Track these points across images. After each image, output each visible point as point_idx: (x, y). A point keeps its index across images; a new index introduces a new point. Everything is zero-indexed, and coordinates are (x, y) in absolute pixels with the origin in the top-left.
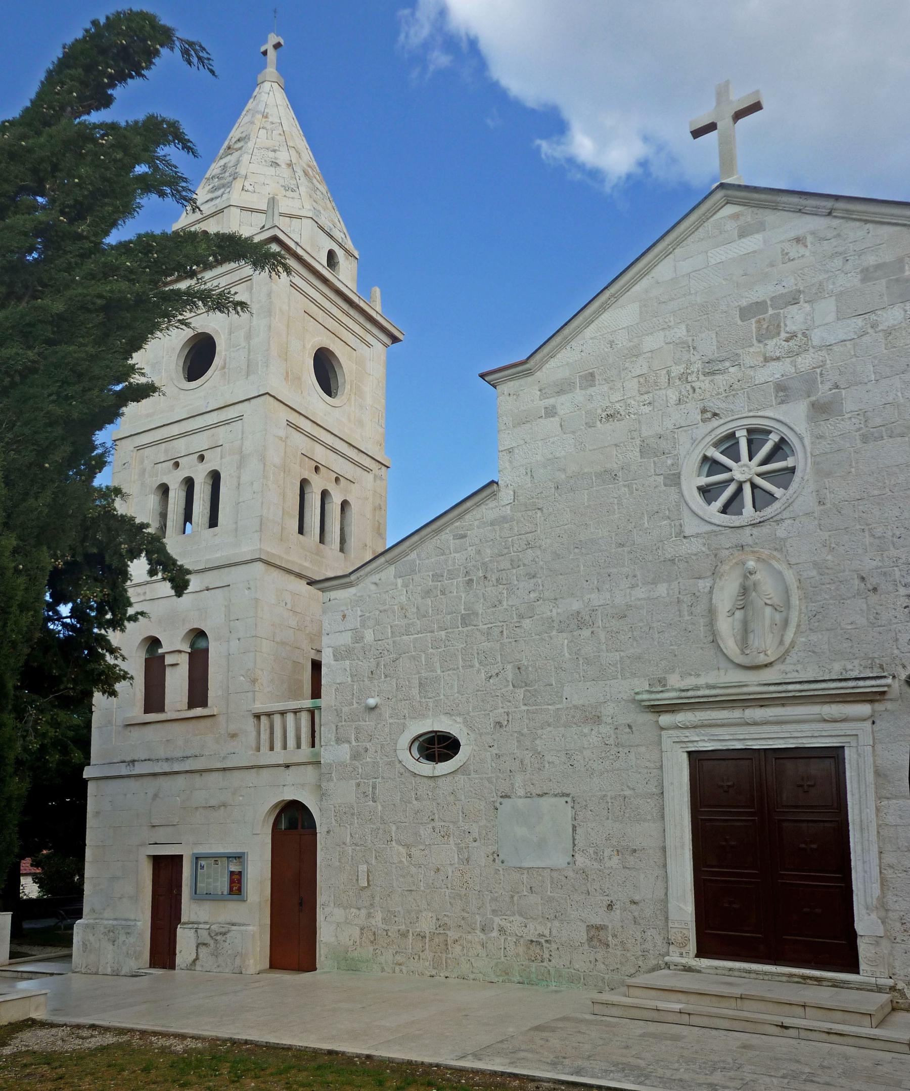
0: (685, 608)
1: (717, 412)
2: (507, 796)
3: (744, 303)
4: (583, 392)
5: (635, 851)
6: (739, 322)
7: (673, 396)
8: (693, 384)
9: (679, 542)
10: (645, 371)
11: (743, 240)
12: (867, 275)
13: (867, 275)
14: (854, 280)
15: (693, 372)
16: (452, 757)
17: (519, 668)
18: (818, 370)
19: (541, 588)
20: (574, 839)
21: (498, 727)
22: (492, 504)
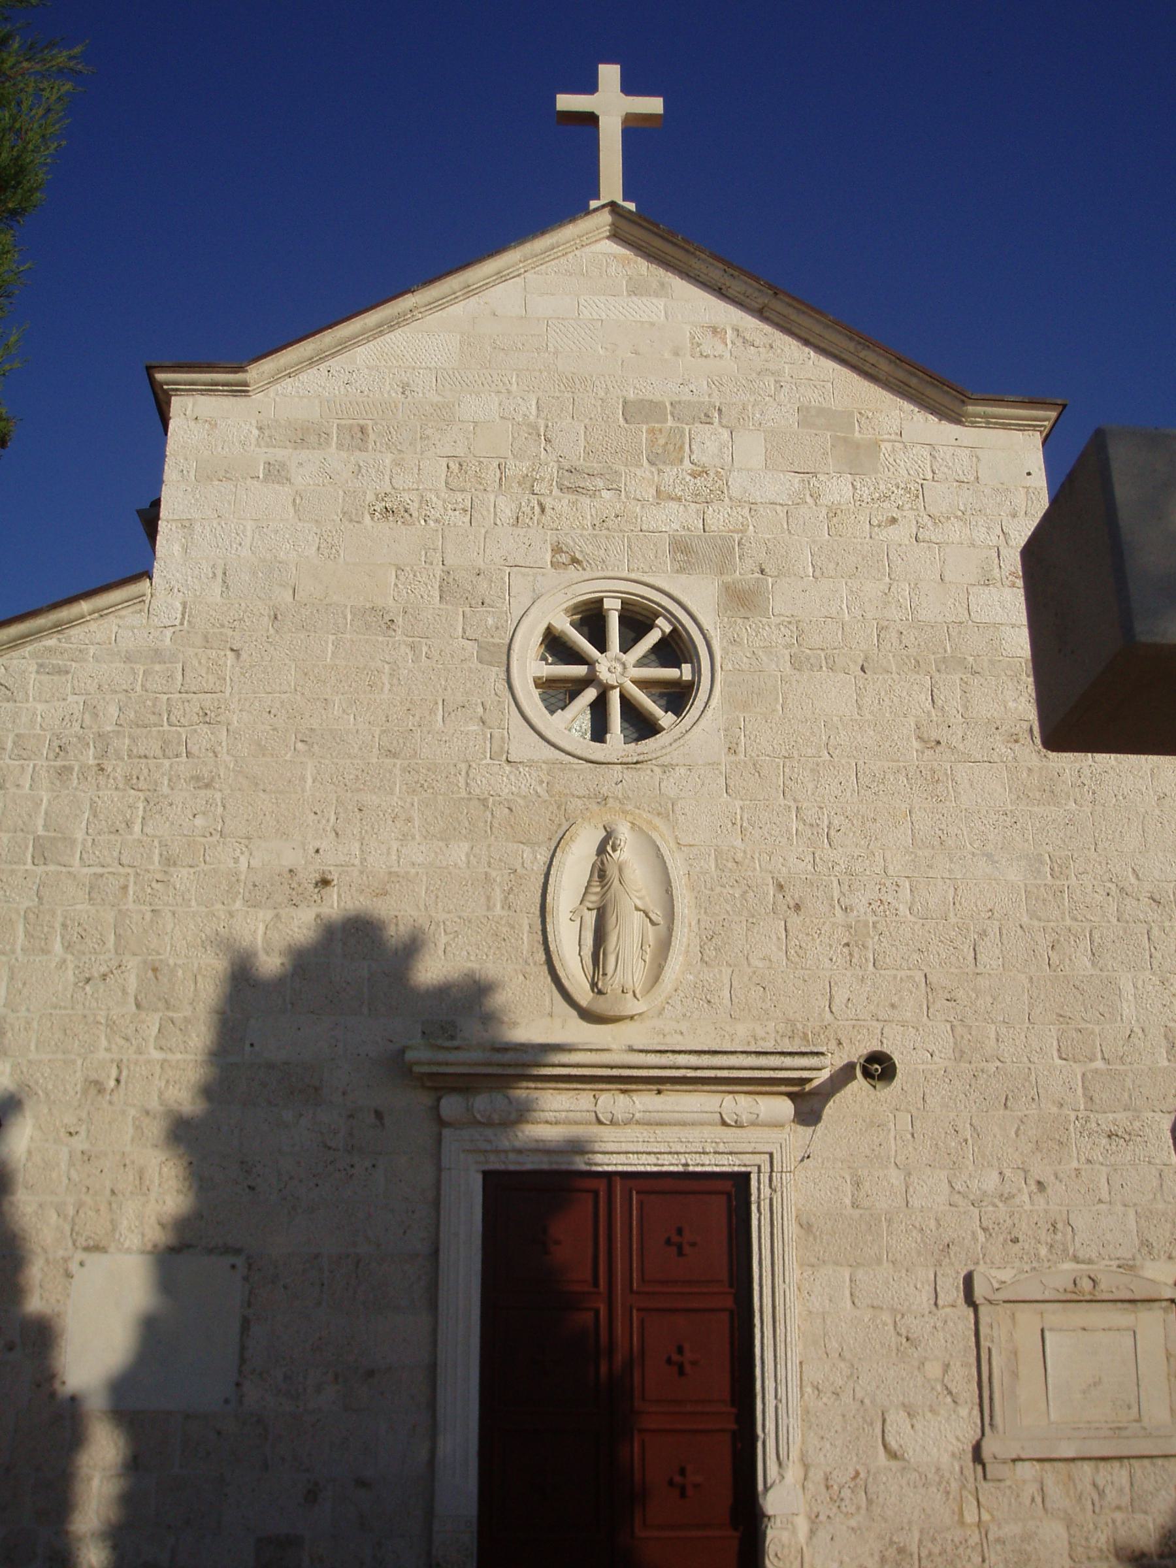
0: (498, 895)
1: (578, 556)
2: (97, 1249)
4: (344, 454)
5: (371, 1373)
7: (507, 510)
8: (542, 499)
9: (495, 769)
10: (460, 451)
11: (634, 298)
15: (543, 479)
16: (894, 1064)
17: (155, 970)
18: (737, 537)
19: (220, 810)
20: (243, 1348)
21: (93, 1091)
22: (131, 617)
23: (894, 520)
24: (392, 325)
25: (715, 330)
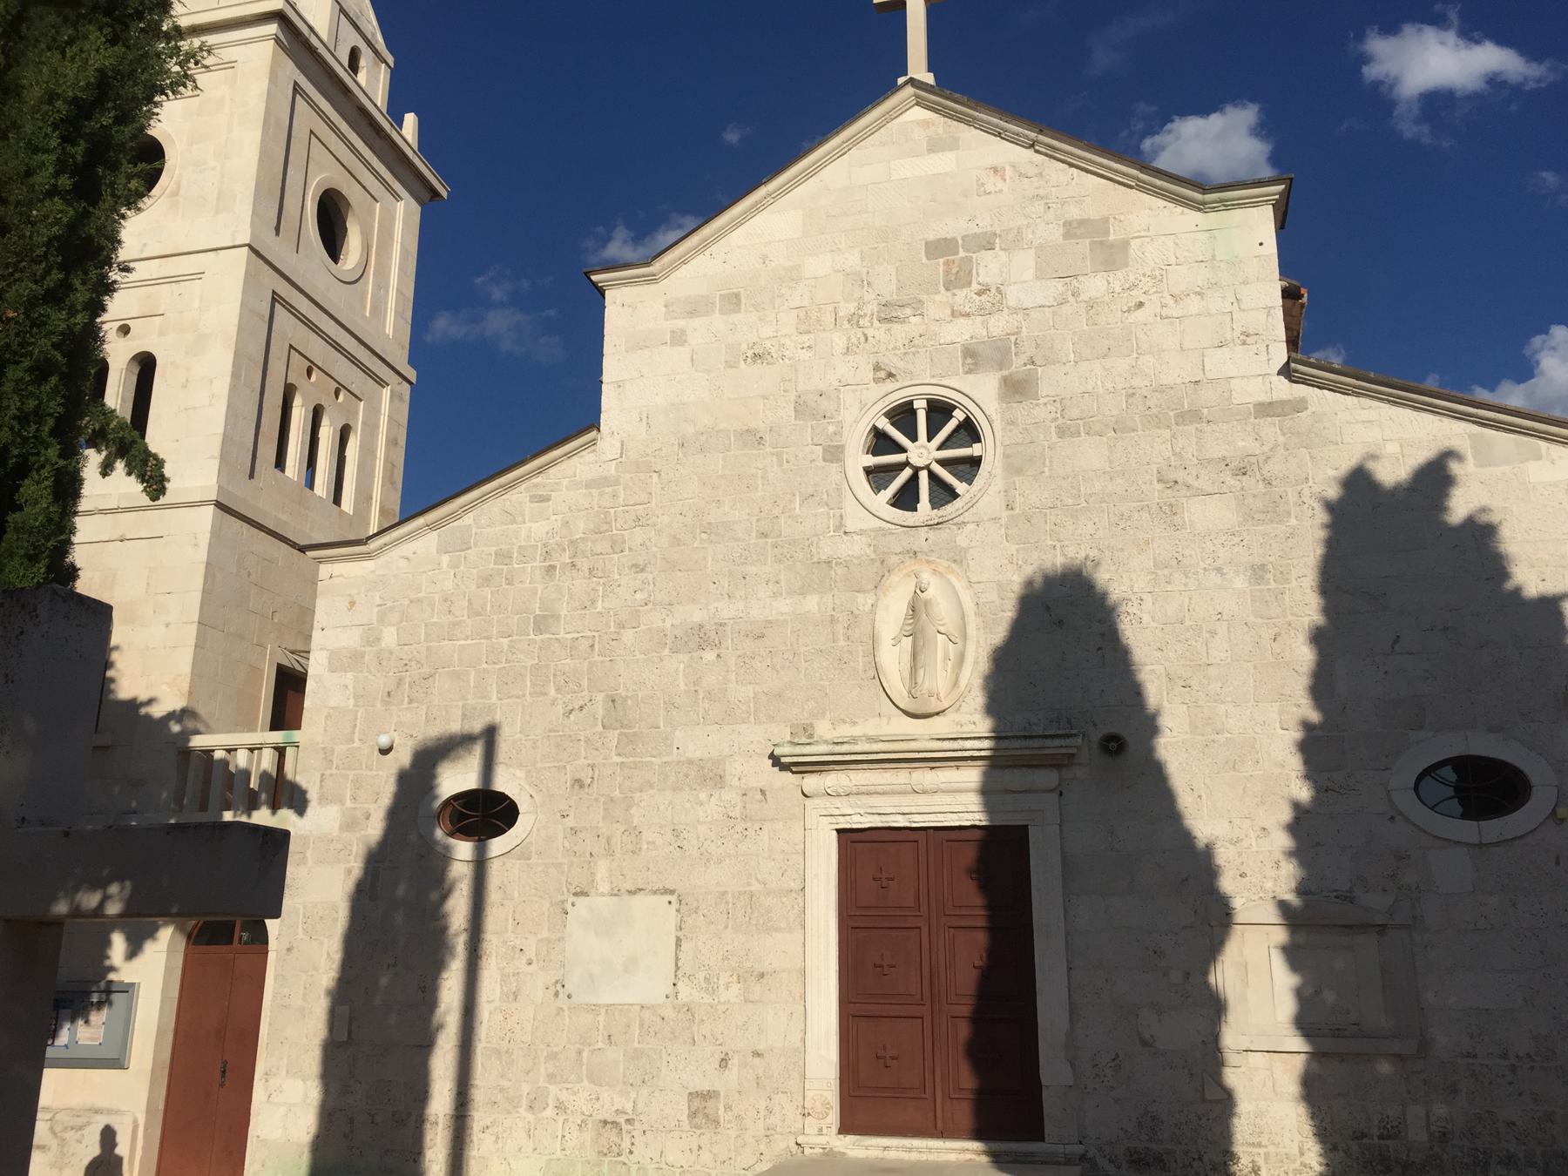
3: (931, 237)
6: (924, 260)
12: (1072, 229)
13: (1072, 229)
14: (1055, 234)
22: (587, 456)
23: (1141, 304)
24: (757, 209)
25: (995, 170)
